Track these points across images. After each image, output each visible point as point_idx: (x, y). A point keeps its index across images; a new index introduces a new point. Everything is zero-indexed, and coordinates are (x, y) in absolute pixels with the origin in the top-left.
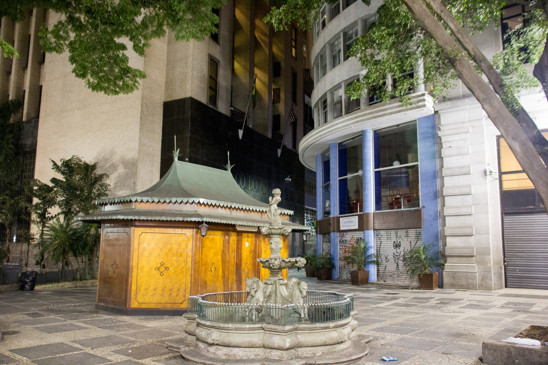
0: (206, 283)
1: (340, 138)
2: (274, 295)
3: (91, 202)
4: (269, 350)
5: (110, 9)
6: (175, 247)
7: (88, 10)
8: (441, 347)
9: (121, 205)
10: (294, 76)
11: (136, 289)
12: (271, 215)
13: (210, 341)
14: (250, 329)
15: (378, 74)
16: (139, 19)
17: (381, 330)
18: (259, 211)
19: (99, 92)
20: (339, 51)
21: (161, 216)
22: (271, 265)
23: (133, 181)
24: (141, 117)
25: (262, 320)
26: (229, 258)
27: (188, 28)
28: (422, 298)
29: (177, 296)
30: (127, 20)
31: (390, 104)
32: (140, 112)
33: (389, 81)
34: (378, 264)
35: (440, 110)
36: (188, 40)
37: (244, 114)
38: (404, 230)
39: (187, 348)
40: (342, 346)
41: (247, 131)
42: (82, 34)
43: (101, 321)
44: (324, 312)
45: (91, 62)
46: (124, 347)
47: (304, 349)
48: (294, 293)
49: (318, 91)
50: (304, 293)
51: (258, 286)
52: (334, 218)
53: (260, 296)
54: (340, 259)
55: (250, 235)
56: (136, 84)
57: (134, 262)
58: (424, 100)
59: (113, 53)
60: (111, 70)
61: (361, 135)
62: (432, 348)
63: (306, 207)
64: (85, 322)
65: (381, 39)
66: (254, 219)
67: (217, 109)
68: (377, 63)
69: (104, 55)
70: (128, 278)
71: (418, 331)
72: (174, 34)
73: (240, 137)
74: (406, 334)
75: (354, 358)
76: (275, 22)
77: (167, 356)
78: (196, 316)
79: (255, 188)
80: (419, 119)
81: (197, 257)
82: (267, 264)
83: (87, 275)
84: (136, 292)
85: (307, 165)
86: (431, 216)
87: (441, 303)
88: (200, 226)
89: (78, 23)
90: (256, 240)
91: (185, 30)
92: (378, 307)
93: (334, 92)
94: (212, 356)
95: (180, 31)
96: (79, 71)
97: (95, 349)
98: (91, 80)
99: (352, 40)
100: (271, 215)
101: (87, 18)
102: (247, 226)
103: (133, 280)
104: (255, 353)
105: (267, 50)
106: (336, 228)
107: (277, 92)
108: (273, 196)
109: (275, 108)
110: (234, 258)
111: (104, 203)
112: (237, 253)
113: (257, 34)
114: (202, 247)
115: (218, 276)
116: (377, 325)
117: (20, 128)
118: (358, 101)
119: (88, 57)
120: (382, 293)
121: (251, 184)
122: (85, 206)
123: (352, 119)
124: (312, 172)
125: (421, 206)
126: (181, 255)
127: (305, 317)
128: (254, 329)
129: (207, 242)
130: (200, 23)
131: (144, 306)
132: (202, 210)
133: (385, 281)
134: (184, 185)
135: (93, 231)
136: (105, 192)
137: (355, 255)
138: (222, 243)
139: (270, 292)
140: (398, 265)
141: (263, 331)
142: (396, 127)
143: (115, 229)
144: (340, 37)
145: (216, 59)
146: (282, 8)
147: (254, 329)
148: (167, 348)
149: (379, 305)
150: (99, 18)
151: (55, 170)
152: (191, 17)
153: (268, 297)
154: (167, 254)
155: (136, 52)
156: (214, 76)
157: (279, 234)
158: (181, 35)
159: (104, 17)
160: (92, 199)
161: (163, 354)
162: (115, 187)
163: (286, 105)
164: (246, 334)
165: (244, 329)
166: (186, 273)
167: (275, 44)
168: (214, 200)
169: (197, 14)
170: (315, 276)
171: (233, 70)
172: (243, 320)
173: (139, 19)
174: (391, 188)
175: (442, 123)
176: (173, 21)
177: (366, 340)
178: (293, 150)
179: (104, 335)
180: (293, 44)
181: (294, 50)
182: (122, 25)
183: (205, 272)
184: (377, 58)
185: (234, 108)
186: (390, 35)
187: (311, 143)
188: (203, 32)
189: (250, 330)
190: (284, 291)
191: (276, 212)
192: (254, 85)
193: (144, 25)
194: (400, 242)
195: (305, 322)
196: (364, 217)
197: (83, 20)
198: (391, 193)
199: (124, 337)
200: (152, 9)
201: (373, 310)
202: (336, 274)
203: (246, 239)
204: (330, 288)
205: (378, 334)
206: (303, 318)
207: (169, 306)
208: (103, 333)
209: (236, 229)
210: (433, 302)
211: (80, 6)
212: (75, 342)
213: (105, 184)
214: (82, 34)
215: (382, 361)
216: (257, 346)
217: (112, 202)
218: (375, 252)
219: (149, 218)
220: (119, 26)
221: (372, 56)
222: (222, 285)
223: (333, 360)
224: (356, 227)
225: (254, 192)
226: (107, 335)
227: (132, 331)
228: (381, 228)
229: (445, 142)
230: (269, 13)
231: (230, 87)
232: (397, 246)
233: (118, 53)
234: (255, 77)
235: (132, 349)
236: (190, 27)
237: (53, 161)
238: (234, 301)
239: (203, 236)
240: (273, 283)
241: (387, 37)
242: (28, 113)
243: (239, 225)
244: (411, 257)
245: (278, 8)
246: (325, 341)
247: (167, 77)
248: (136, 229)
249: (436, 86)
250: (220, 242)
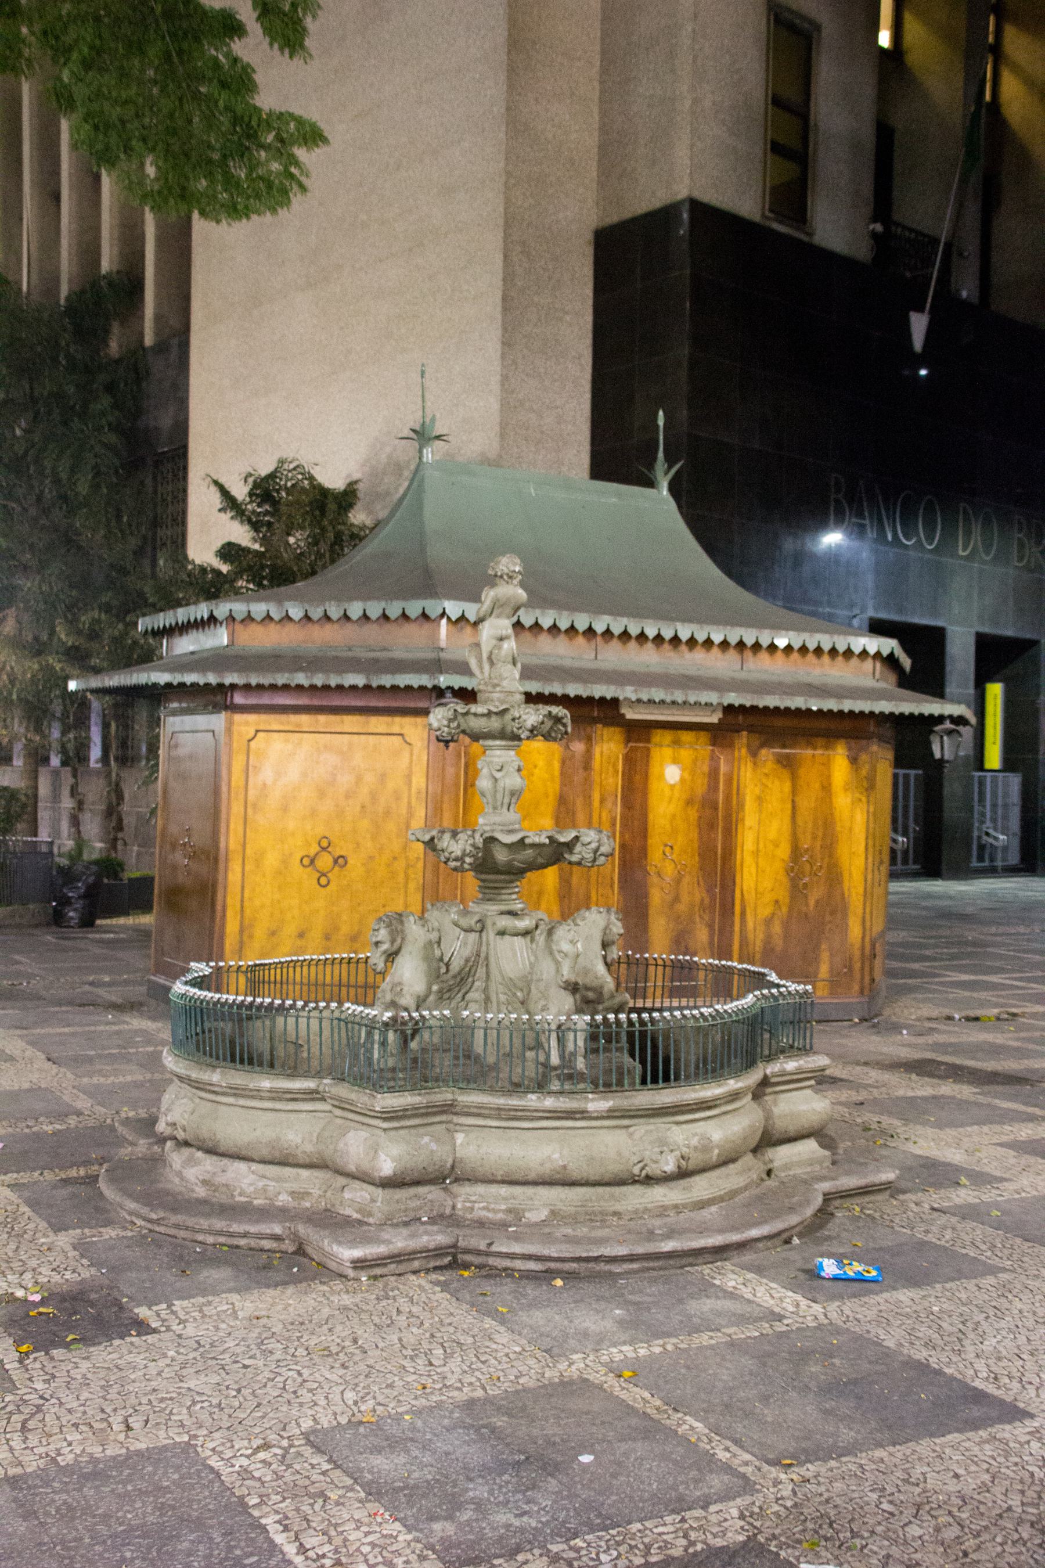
11: (242, 931)
14: (276, 1095)
24: (504, 299)
32: (500, 276)
47: (481, 1189)
55: (687, 736)
57: (231, 839)
67: (810, 235)
79: (987, 549)
84: (241, 943)
90: (714, 759)
103: (229, 901)
104: (295, 1186)
110: (614, 825)
112: (628, 804)
115: (540, 893)
117: (136, 371)
121: (968, 534)
128: (293, 1096)
138: (557, 765)
147: (293, 1096)
151: (230, 514)
164: (269, 1114)
165: (256, 1094)
189: (280, 1100)
195: (567, 1087)
203: (667, 752)
206: (555, 1068)
209: (623, 715)
216: (301, 1162)
223: (564, 1247)
225: (985, 562)
231: (868, 134)
237: (216, 483)
238: (233, 988)
242: (158, 318)
246: (564, 1167)
247: (604, 129)
248: (238, 718)
250: (549, 764)
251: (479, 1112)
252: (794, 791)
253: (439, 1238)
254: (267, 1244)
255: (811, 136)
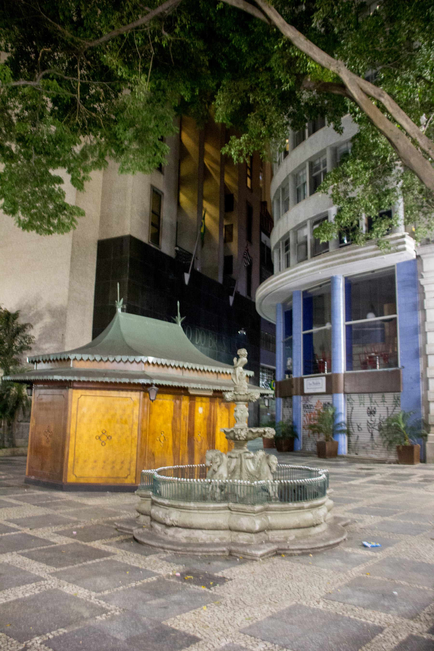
0: (153, 455)
1: (306, 285)
2: (238, 470)
3: (12, 356)
4: (235, 533)
5: (45, 137)
6: (119, 412)
7: (19, 138)
8: (428, 532)
9: (56, 363)
10: (250, 210)
11: (74, 462)
12: (236, 379)
13: (168, 522)
14: (215, 509)
15: (352, 214)
16: (77, 149)
17: (358, 511)
18: (215, 372)
19: (30, 231)
20: (304, 184)
21: (104, 377)
22: (237, 436)
23: (60, 333)
24: (72, 258)
25: (225, 499)
26: (181, 425)
27: (134, 159)
28: (402, 475)
29: (121, 469)
30: (65, 150)
31: (364, 247)
33: (363, 222)
34: (348, 433)
35: (423, 254)
36: (133, 172)
37: (190, 255)
38: (379, 394)
39: (141, 530)
40: (317, 530)
41: (195, 275)
42: (13, 165)
43: (34, 497)
44: (294, 491)
45: (21, 197)
46: (67, 528)
47: (275, 532)
48: (262, 468)
49: (279, 229)
50: (274, 468)
51: (222, 460)
52: (297, 379)
53: (223, 471)
54: (304, 427)
55: (204, 399)
56: (73, 223)
57: (71, 430)
58: (404, 243)
59: (48, 187)
60: (45, 206)
61: (330, 282)
62: (418, 533)
63: (262, 364)
64: (16, 499)
65: (356, 173)
66: (208, 380)
67: (160, 248)
68: (351, 201)
69: (37, 189)
70: (65, 447)
71: (401, 514)
72: (118, 165)
73: (187, 282)
74: (387, 516)
75: (331, 542)
76: (234, 154)
77: (118, 539)
78: (151, 493)
79: (203, 342)
80: (398, 264)
81: (145, 425)
82: (232, 435)
83: (6, 443)
84: (74, 465)
85: (265, 315)
86: (411, 378)
87: (425, 481)
88: (149, 389)
89: (8, 153)
91: (131, 162)
92: (351, 485)
93: (299, 232)
94: (170, 539)
95: (125, 162)
96: (8, 207)
97: (34, 530)
98: (22, 218)
99: (319, 172)
100: (236, 379)
101: (19, 147)
102: (202, 389)
103: (70, 451)
104: (220, 536)
105: (218, 181)
106: (299, 391)
107: (229, 229)
108: (238, 357)
109: (226, 248)
111: (37, 360)
112: (190, 420)
113: (207, 162)
114: (151, 413)
115: (168, 447)
116: (353, 506)
118: (326, 245)
119: (19, 192)
120: (354, 468)
121: (198, 337)
122: (5, 360)
123: (320, 263)
124: (270, 324)
125: (400, 365)
126: (126, 422)
127: (275, 496)
128: (219, 509)
129: (156, 408)
130: (148, 153)
131: (82, 481)
132: (151, 370)
133: (356, 454)
134: (129, 341)
135: (14, 391)
136: (29, 345)
137: (322, 423)
138: (172, 407)
139: (235, 467)
140: (372, 435)
141: (229, 511)
142: (371, 273)
143: (50, 391)
144: (305, 168)
145: (159, 191)
146: (242, 138)
147: (219, 509)
148: (116, 529)
149: (352, 482)
150: (33, 147)
152: (138, 147)
153: (232, 473)
154: (109, 421)
155: (75, 186)
156: (156, 211)
157: (245, 401)
158: (126, 167)
159: (38, 147)
160: (13, 353)
161: (114, 536)
162: (40, 340)
163: (240, 245)
165: (208, 509)
166: (132, 442)
167: (228, 173)
168: (164, 358)
169: (145, 142)
170: (274, 447)
171: (179, 204)
172: (204, 498)
173: (77, 149)
174: (364, 344)
175: (425, 269)
176: (117, 151)
177: (343, 523)
178: (248, 297)
179: (41, 514)
180: (249, 173)
181: (249, 180)
182: (58, 155)
183: (153, 442)
184: (351, 195)
185: (179, 247)
186: (366, 168)
187: (270, 290)
188: (151, 164)
190: (251, 466)
191: (242, 375)
192: (203, 221)
193: (84, 155)
194: (375, 409)
196: (333, 377)
197: (14, 149)
198: (364, 349)
199: (64, 516)
200: (92, 137)
201: (345, 487)
202: (299, 444)
204: (292, 461)
205: (355, 516)
207: (111, 482)
208: (40, 511)
210: (415, 480)
211: (11, 133)
212: (9, 521)
213: (28, 336)
214: (13, 165)
215: (363, 547)
217: (46, 360)
218: (346, 419)
219: (91, 379)
220: (54, 156)
221: (346, 193)
222: (172, 457)
224: (324, 390)
226: (44, 514)
227: (72, 510)
228: (353, 391)
229: (428, 292)
230: (228, 144)
231: (174, 223)
232: (371, 412)
233: (53, 186)
234: (203, 212)
235: (77, 530)
236: (136, 158)
239: (152, 401)
240: (238, 456)
241: (364, 172)
243: (193, 388)
244: (389, 426)
245: (239, 137)
248: (75, 391)
249: (419, 227)
251: (275, 510)
252: (229, 415)
253: (274, 547)
254: (219, 554)
255: (161, 222)
